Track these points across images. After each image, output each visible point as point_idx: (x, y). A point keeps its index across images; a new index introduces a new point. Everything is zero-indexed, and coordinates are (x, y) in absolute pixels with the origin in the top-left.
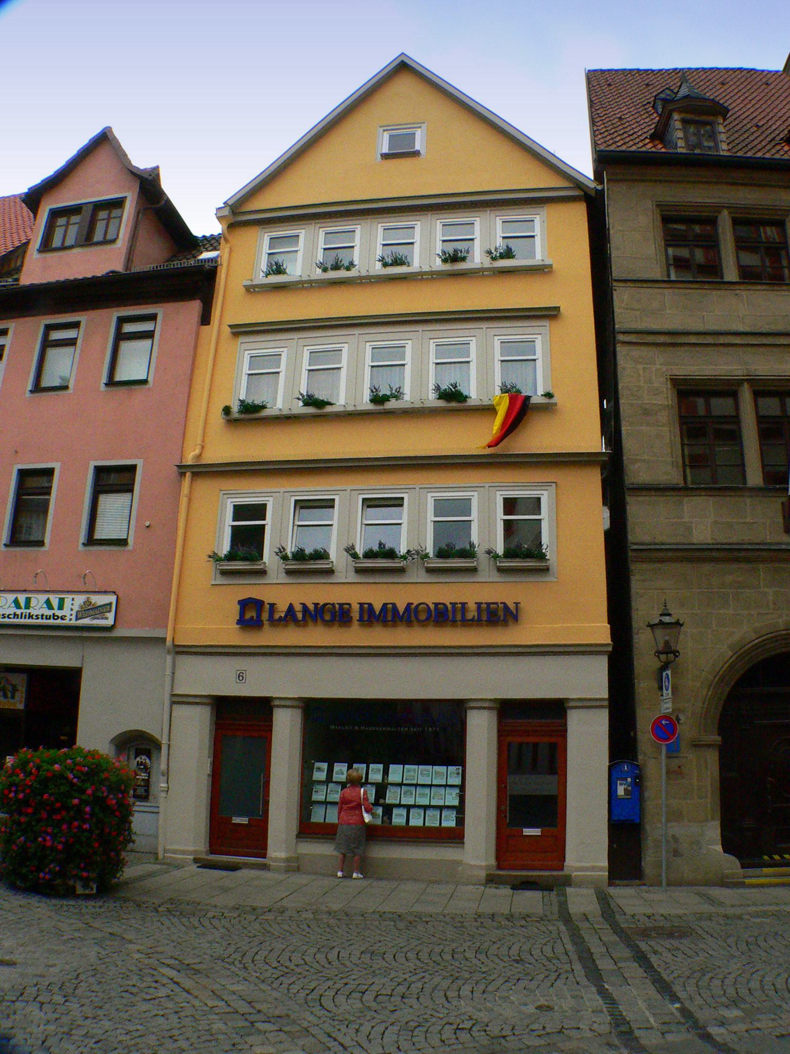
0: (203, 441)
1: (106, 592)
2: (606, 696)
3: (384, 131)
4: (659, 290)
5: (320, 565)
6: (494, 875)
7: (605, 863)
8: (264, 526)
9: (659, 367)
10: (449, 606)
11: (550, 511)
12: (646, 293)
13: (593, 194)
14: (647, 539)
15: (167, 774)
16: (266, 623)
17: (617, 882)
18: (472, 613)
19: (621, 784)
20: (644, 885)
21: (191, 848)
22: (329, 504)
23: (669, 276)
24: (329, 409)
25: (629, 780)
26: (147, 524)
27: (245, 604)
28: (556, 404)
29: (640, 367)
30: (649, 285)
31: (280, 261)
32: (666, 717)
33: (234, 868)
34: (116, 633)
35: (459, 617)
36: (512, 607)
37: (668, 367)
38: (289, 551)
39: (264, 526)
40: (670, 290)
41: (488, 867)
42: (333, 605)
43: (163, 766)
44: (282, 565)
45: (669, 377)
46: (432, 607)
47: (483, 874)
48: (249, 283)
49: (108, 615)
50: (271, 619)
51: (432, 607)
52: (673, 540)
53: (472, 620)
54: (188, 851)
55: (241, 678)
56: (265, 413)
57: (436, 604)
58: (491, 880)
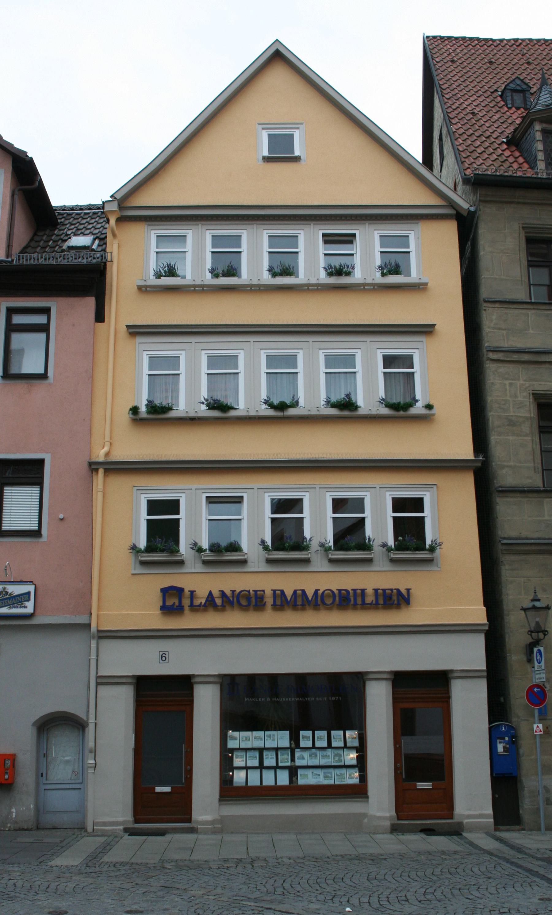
0: (111, 439)
1: (21, 582)
2: (484, 668)
3: (263, 129)
4: (524, 311)
5: (235, 556)
6: (397, 824)
7: (490, 811)
8: (178, 520)
9: (522, 382)
10: (351, 592)
11: (432, 507)
12: (512, 312)
13: (465, 214)
14: (513, 534)
15: (94, 751)
16: (186, 608)
17: (501, 827)
18: (370, 599)
19: (500, 743)
20: (523, 829)
21: (121, 819)
22: (239, 500)
23: (531, 299)
24: (232, 413)
25: (507, 739)
26: (61, 516)
27: (166, 592)
28: (434, 415)
29: (507, 382)
30: (515, 306)
31: (173, 263)
32: (537, 686)
33: (162, 833)
34: (36, 621)
35: (359, 601)
36: (404, 592)
37: (531, 383)
38: (205, 545)
39: (178, 520)
40: (533, 311)
41: (391, 818)
42: (249, 591)
43: (91, 744)
44: (265, 555)
45: (531, 392)
46: (336, 592)
47: (387, 824)
48: (142, 283)
49: (27, 603)
50: (192, 605)
51: (336, 592)
52: (536, 535)
53: (371, 604)
54: (117, 822)
55: (164, 659)
56: (172, 414)
57: (340, 591)
58: (394, 829)
